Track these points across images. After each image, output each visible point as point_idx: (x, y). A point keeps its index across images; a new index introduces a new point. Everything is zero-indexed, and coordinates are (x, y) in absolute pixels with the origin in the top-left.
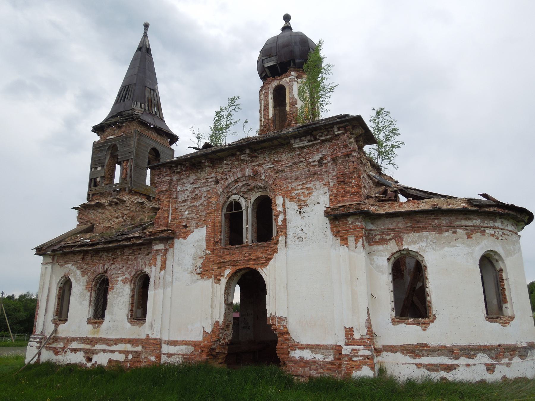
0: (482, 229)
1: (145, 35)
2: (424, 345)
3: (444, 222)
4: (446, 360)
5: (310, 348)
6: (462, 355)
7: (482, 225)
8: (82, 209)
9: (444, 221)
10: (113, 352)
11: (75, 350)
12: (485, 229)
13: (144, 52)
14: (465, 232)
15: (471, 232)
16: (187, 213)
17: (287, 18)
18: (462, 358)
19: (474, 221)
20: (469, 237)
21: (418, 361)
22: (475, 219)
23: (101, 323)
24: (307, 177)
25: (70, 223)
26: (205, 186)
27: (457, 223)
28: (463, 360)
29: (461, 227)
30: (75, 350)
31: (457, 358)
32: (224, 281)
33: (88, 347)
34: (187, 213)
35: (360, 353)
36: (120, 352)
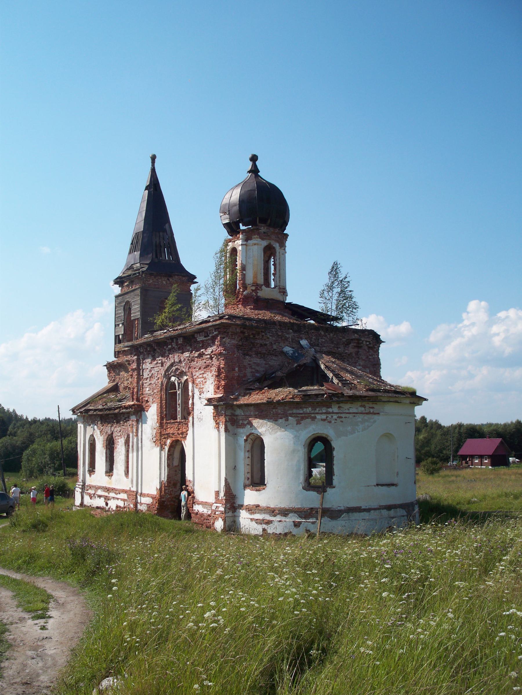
0: (313, 415)
1: (153, 170)
2: (258, 506)
3: (280, 411)
4: (268, 517)
5: (202, 504)
6: (279, 514)
7: (313, 412)
8: (111, 367)
9: (280, 410)
10: (118, 499)
11: (100, 496)
12: (316, 415)
13: (154, 189)
14: (295, 419)
15: (300, 419)
16: (148, 389)
17: (254, 159)
18: (278, 516)
19: (305, 410)
20: (298, 423)
21: (252, 517)
22: (306, 408)
23: (112, 475)
24: (205, 368)
25: (101, 381)
26: (157, 367)
27: (290, 412)
28: (278, 518)
29: (291, 415)
30: (100, 496)
31: (275, 516)
32: (167, 448)
33: (106, 494)
34: (148, 389)
35: (219, 509)
36: (122, 499)
